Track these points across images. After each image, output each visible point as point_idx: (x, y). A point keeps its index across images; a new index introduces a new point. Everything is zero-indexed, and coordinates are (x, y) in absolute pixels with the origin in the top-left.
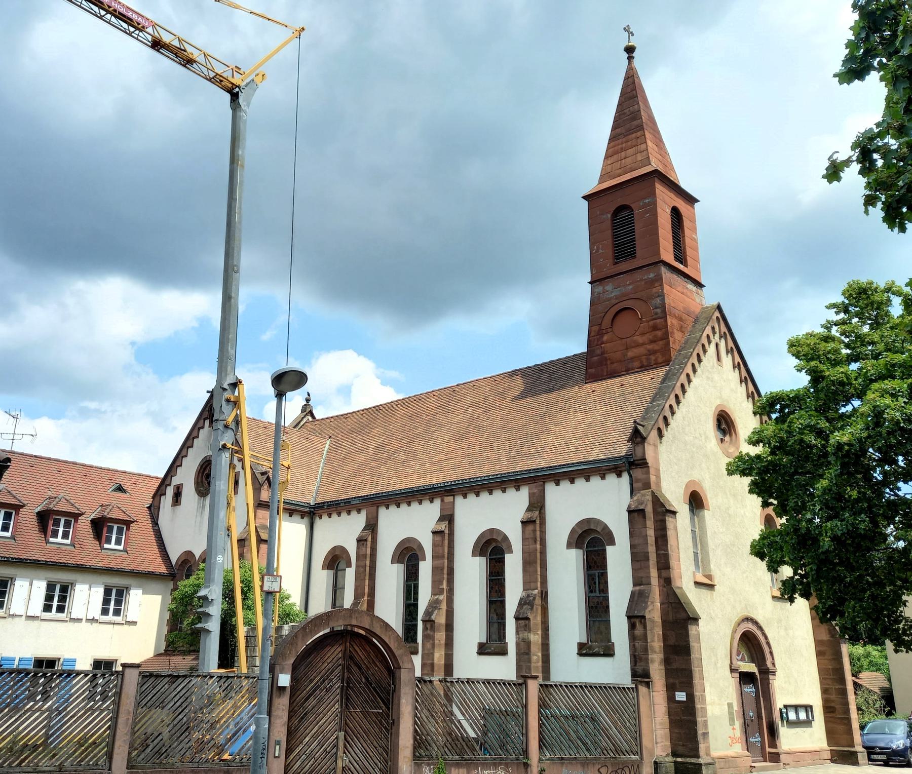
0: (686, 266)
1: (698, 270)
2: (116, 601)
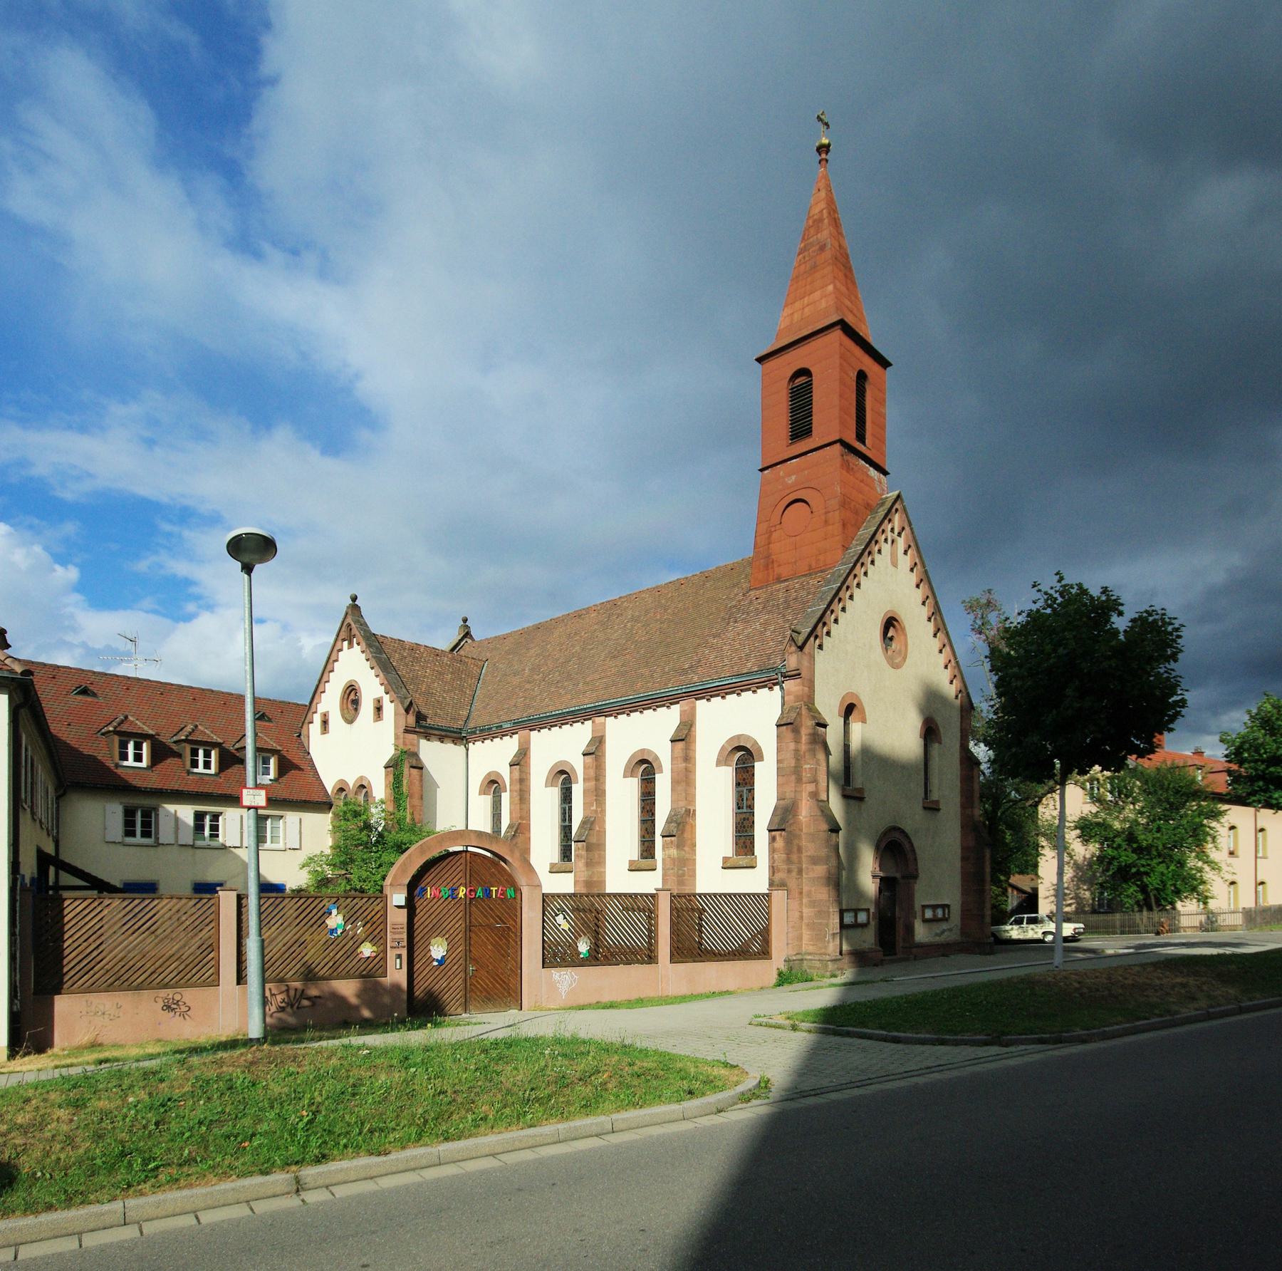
0: (864, 443)
1: (883, 454)
2: (211, 826)
